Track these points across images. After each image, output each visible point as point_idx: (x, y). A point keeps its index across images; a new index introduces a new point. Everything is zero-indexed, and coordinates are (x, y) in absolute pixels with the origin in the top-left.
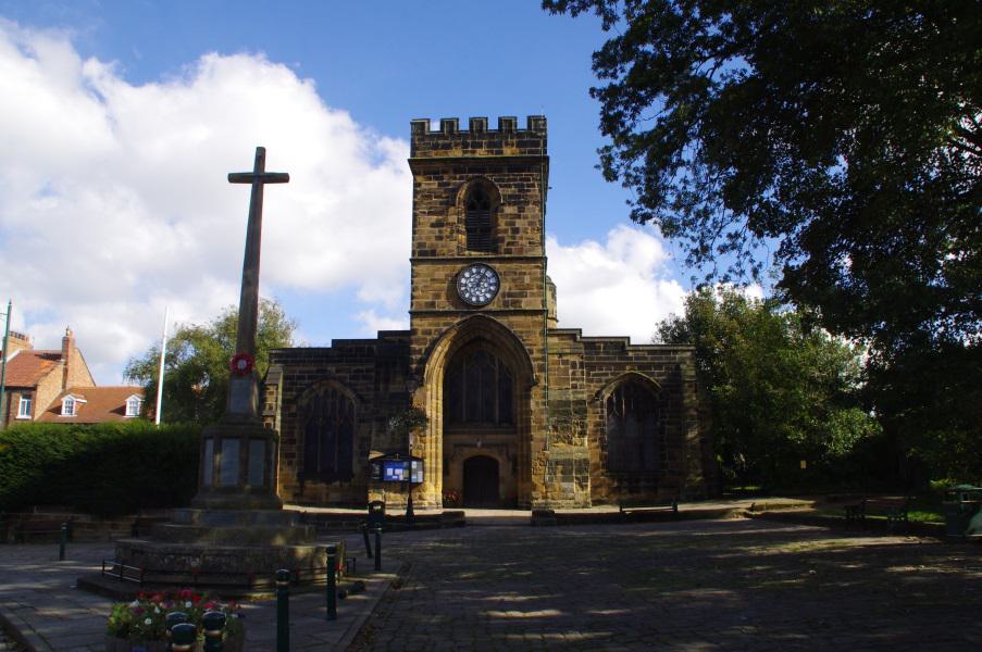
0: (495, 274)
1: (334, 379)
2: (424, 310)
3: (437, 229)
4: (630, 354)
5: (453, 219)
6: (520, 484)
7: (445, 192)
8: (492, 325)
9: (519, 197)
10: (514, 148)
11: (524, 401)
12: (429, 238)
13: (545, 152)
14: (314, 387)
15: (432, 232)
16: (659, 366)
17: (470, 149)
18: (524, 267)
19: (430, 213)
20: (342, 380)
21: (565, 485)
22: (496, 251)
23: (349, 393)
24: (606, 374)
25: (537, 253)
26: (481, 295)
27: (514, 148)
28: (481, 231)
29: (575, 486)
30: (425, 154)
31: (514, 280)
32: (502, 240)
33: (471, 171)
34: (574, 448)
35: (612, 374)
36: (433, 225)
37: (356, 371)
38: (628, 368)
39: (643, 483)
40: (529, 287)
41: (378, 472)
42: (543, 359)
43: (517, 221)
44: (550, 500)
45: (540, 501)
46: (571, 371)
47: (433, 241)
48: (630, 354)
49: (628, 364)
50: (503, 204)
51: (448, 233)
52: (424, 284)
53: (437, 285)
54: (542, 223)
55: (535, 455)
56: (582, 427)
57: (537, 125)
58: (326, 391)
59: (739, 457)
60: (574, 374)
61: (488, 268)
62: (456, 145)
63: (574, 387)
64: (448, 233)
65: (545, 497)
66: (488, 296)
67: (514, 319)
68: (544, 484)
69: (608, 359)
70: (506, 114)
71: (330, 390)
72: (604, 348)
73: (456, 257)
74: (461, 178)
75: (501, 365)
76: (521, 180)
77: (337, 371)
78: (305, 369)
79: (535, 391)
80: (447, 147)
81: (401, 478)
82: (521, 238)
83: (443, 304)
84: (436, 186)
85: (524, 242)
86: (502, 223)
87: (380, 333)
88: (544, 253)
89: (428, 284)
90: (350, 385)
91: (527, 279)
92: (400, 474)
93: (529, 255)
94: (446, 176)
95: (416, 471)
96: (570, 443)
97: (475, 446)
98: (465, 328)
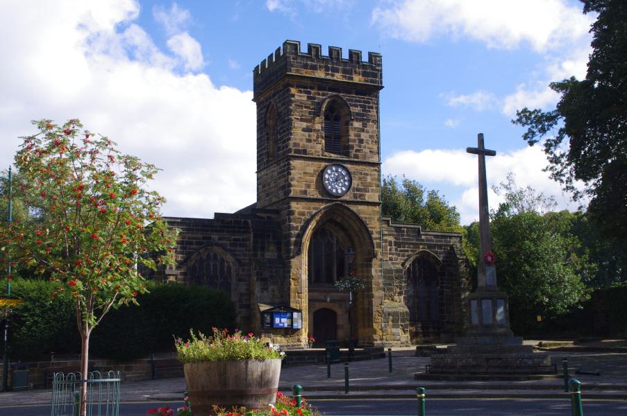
0: (349, 173)
1: (217, 245)
2: (300, 196)
3: (307, 134)
4: (423, 237)
5: (318, 127)
6: (361, 331)
7: (312, 104)
8: (345, 211)
9: (363, 115)
10: (360, 76)
11: (366, 269)
12: (301, 140)
13: (381, 83)
14: (201, 251)
15: (303, 135)
16: (440, 247)
17: (330, 72)
18: (368, 169)
19: (302, 120)
20: (223, 247)
21: (394, 330)
22: (347, 155)
23: (229, 258)
24: (408, 251)
25: (375, 160)
26: (339, 188)
27: (360, 76)
28: (335, 138)
29: (399, 331)
30: (297, 71)
31: (360, 179)
32: (353, 147)
33: (330, 90)
34: (396, 304)
35: (412, 251)
36: (304, 130)
37: (234, 240)
38: (421, 247)
39: (431, 330)
40: (370, 185)
41: (269, 322)
42: (380, 238)
43: (362, 134)
44: (384, 341)
45: (379, 342)
46: (389, 248)
47: (304, 142)
48: (423, 237)
49: (421, 244)
50: (352, 120)
51: (315, 138)
52: (299, 176)
53: (308, 178)
54: (378, 137)
55: (375, 309)
56: (400, 289)
57: (375, 58)
58: (208, 255)
59: (495, 307)
60: (390, 249)
61: (344, 168)
62: (320, 67)
63: (391, 259)
64: (315, 138)
65: (382, 339)
66: (344, 189)
67: (361, 207)
68: (381, 329)
69: (409, 239)
70: (314, 41)
71: (212, 254)
72: (407, 232)
73: (321, 157)
74: (323, 95)
75: (337, 241)
76: (364, 102)
77: (220, 239)
78: (195, 236)
79: (375, 261)
80: (314, 68)
81: (286, 325)
82: (365, 147)
83: (313, 193)
84: (305, 99)
85: (367, 150)
86: (352, 137)
87: (216, 214)
88: (380, 160)
89: (302, 176)
90: (230, 251)
91: (369, 179)
92: (285, 322)
93: (371, 160)
94: (313, 91)
95: (297, 319)
96: (393, 300)
97: (326, 301)
98: (328, 212)
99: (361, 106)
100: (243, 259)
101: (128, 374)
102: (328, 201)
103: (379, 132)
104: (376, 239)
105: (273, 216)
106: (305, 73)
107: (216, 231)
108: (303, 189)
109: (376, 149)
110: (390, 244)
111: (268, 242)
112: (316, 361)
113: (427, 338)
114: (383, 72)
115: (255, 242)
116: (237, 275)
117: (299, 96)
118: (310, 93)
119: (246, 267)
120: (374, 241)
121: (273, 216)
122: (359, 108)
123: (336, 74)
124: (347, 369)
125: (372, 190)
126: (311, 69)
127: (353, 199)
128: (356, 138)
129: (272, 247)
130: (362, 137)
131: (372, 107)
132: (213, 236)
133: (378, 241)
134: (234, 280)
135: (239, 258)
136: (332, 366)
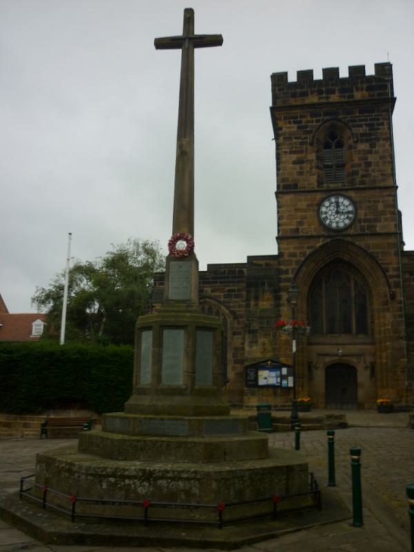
3: (298, 166)
9: (370, 134)
19: (291, 152)
27: (364, 92)
36: (294, 163)
37: (228, 291)
64: (308, 169)
74: (317, 121)
77: (212, 291)
82: (374, 171)
84: (295, 129)
85: (377, 174)
91: (380, 207)
99: (367, 125)
100: (238, 311)
101: (27, 431)
102: (329, 237)
104: (393, 276)
108: (294, 227)
109: (390, 170)
111: (263, 292)
116: (232, 328)
122: (364, 127)
127: (359, 232)
128: (362, 162)
129: (268, 295)
130: (369, 160)
132: (205, 289)
133: (396, 279)
135: (233, 309)
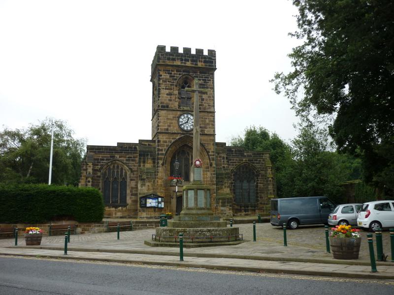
3: (169, 96)
9: (204, 85)
19: (166, 89)
35: (238, 162)
36: (167, 94)
37: (128, 157)
39: (250, 208)
40: (208, 124)
47: (168, 101)
60: (223, 162)
62: (178, 59)
74: (180, 74)
80: (174, 60)
82: (205, 103)
84: (168, 77)
89: (166, 120)
93: (209, 110)
99: (203, 80)
103: (214, 94)
104: (211, 155)
105: (151, 144)
106: (168, 62)
107: (118, 153)
108: (166, 128)
110: (224, 158)
111: (148, 159)
112: (154, 227)
113: (247, 213)
114: (216, 60)
115: (140, 159)
116: (130, 177)
117: (164, 76)
118: (171, 74)
119: (135, 173)
120: (210, 157)
121: (151, 144)
122: (202, 81)
123: (187, 62)
124: (254, 227)
125: (209, 127)
126: (172, 60)
129: (150, 161)
131: (210, 80)
134: (128, 180)
136: (120, 232)
